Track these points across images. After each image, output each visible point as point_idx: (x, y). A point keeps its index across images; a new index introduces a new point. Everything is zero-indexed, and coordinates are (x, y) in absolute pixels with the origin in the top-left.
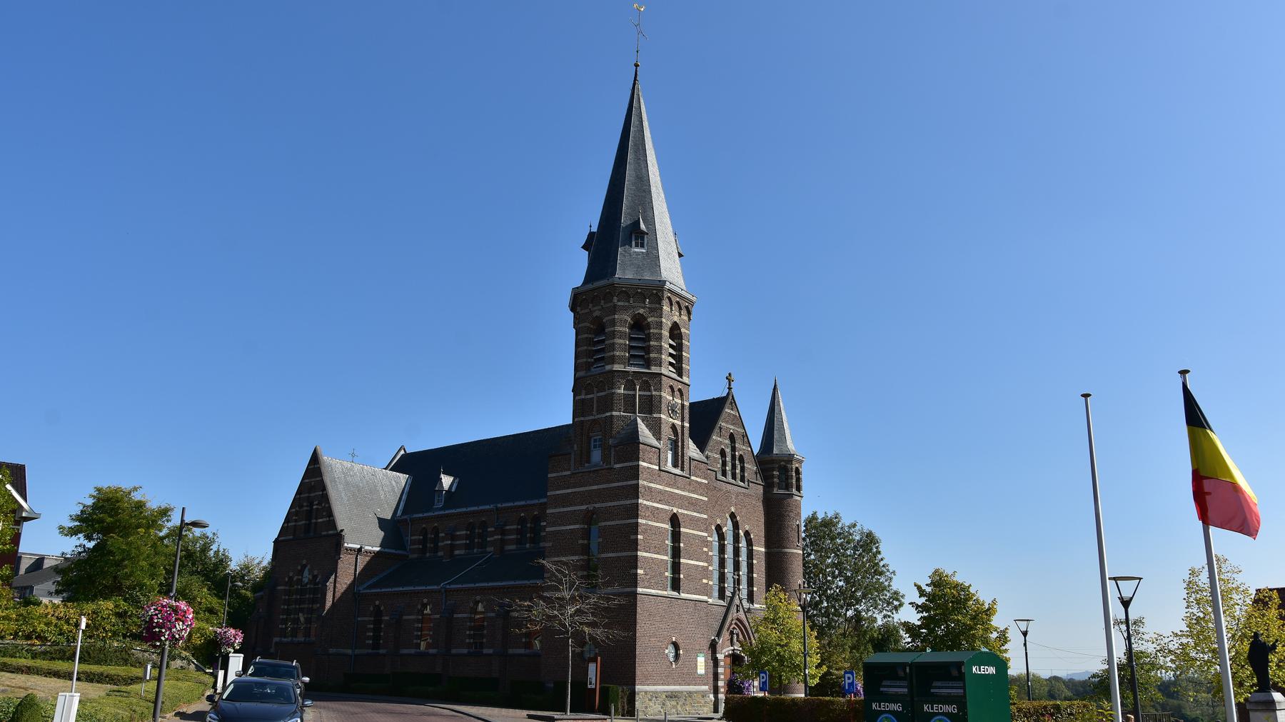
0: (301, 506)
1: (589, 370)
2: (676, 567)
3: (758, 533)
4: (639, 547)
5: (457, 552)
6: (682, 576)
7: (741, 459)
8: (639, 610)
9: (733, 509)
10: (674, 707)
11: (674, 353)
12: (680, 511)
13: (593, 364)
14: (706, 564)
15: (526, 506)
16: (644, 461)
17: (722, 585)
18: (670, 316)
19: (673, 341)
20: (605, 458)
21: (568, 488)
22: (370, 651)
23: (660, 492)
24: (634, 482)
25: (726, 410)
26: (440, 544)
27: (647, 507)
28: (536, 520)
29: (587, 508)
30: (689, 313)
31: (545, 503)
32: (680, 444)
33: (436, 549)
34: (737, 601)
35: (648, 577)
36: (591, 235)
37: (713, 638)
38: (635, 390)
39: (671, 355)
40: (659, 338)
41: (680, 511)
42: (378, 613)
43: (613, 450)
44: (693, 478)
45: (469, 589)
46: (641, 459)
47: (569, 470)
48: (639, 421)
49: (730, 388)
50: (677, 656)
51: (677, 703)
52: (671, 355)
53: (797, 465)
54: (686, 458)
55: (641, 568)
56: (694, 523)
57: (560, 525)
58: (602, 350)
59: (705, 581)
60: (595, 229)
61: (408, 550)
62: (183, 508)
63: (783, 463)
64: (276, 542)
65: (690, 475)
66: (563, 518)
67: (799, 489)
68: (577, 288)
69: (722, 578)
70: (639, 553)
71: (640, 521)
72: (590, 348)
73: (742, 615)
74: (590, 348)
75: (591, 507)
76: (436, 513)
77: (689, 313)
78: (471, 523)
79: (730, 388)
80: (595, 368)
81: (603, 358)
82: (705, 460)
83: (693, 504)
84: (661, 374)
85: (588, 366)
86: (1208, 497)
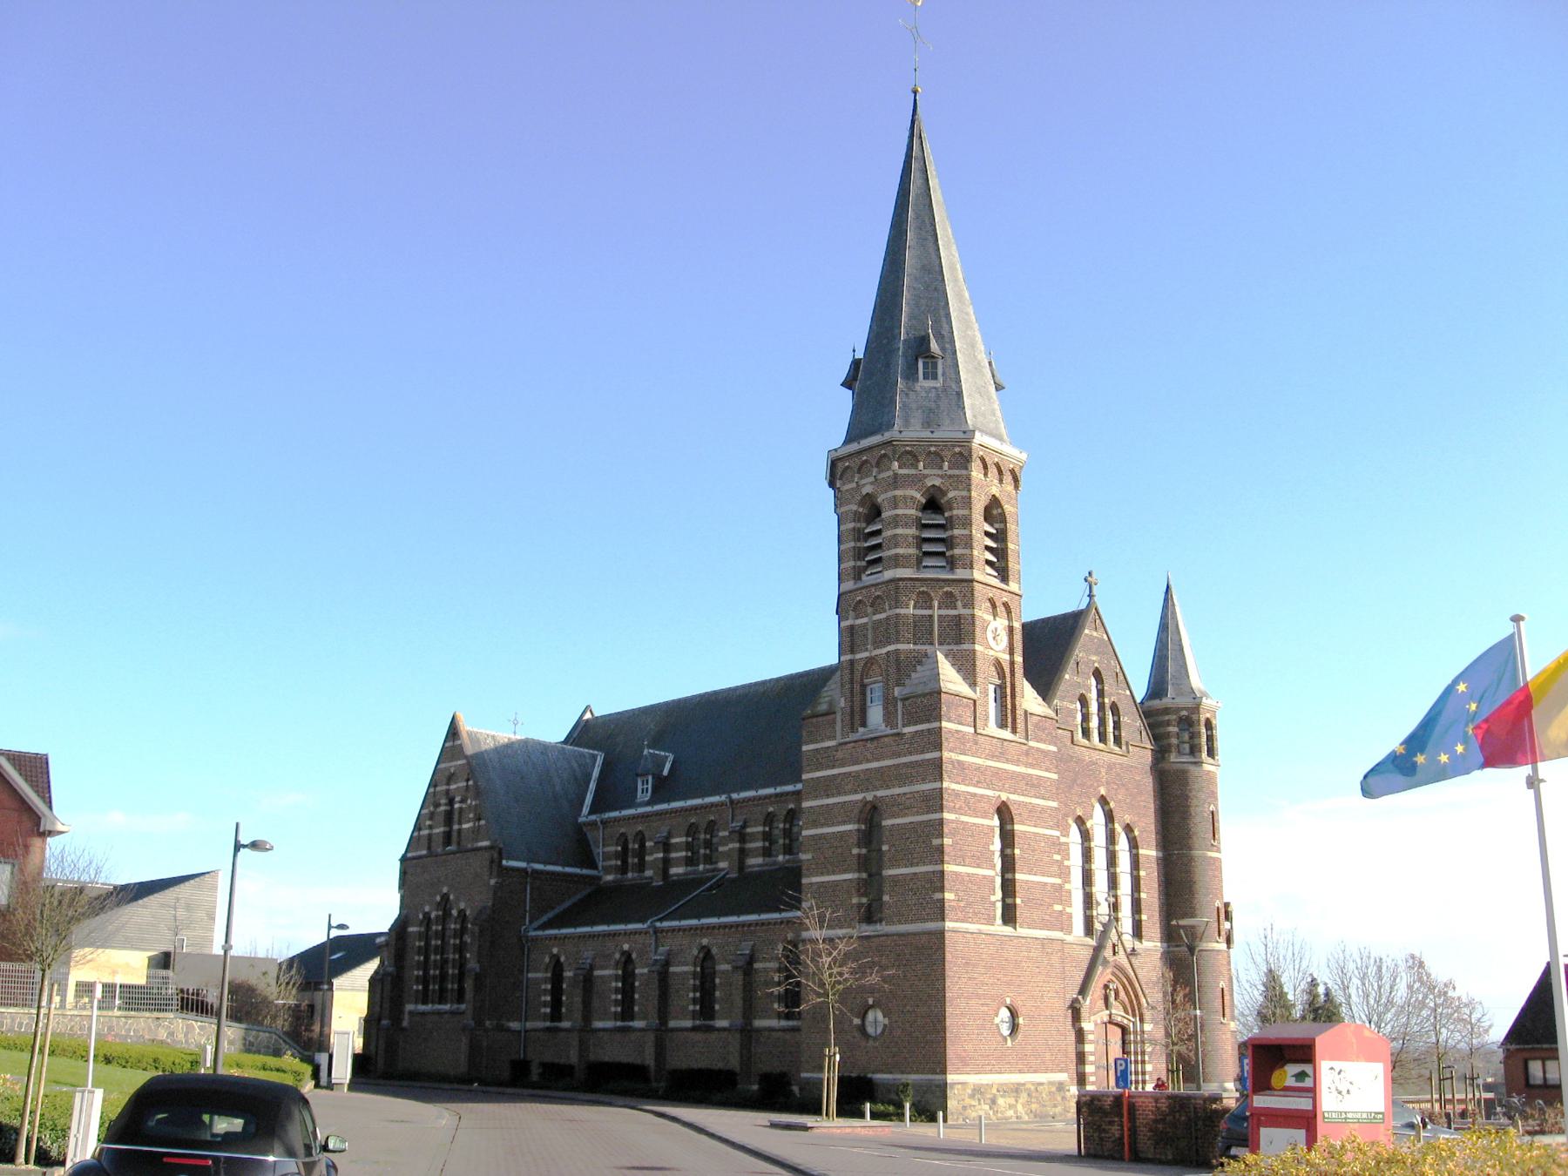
0: (437, 805)
1: (860, 579)
2: (1009, 888)
3: (1147, 827)
4: (946, 858)
5: (674, 871)
6: (1018, 901)
7: (1115, 709)
8: (948, 957)
9: (1103, 791)
10: (1011, 1106)
11: (994, 545)
12: (1013, 797)
13: (866, 568)
14: (1058, 881)
15: (777, 795)
16: (949, 720)
17: (1137, 917)
18: (983, 486)
19: (992, 525)
20: (889, 717)
21: (833, 767)
22: (548, 1024)
23: (978, 768)
24: (935, 755)
25: (1086, 631)
26: (648, 858)
27: (957, 794)
28: (792, 816)
29: (865, 797)
30: (1016, 480)
31: (798, 793)
32: (1008, 691)
33: (641, 866)
34: (1113, 935)
35: (962, 904)
36: (856, 364)
37: (1075, 996)
38: (931, 607)
39: (988, 548)
40: (967, 522)
41: (1013, 797)
42: (557, 968)
43: (900, 704)
44: (1032, 743)
45: (691, 928)
46: (944, 718)
47: (834, 738)
48: (940, 657)
49: (1091, 596)
50: (1014, 1028)
51: (1017, 1101)
52: (988, 548)
53: (1208, 715)
54: (1019, 712)
55: (951, 891)
56: (1036, 815)
57: (822, 825)
58: (878, 547)
59: (1058, 908)
60: (860, 355)
61: (600, 868)
62: (237, 824)
63: (1184, 713)
64: (404, 860)
65: (1027, 739)
66: (827, 815)
67: (1211, 753)
68: (836, 450)
69: (1089, 901)
70: (948, 868)
71: (946, 815)
72: (859, 544)
73: (1121, 958)
74: (859, 544)
75: (869, 797)
76: (641, 810)
77: (1016, 480)
78: (693, 824)
79: (1091, 596)
80: (869, 575)
81: (879, 560)
82: (1053, 714)
83: (1033, 785)
84: (972, 581)
85: (857, 574)
86: (1542, 785)
